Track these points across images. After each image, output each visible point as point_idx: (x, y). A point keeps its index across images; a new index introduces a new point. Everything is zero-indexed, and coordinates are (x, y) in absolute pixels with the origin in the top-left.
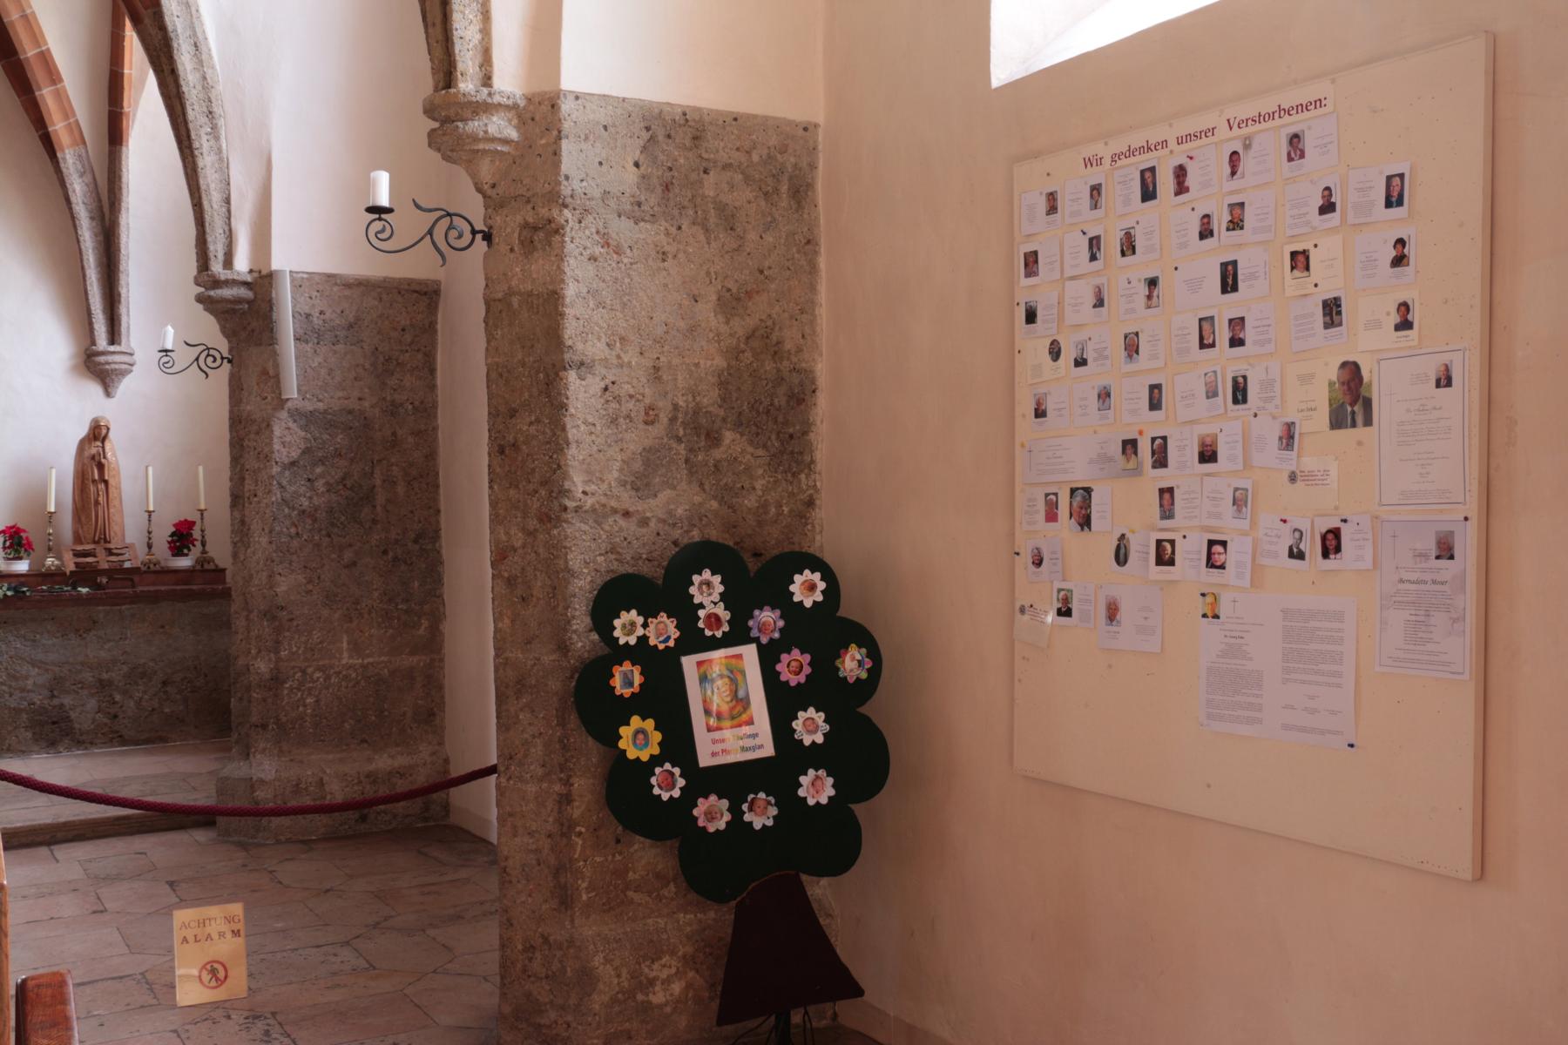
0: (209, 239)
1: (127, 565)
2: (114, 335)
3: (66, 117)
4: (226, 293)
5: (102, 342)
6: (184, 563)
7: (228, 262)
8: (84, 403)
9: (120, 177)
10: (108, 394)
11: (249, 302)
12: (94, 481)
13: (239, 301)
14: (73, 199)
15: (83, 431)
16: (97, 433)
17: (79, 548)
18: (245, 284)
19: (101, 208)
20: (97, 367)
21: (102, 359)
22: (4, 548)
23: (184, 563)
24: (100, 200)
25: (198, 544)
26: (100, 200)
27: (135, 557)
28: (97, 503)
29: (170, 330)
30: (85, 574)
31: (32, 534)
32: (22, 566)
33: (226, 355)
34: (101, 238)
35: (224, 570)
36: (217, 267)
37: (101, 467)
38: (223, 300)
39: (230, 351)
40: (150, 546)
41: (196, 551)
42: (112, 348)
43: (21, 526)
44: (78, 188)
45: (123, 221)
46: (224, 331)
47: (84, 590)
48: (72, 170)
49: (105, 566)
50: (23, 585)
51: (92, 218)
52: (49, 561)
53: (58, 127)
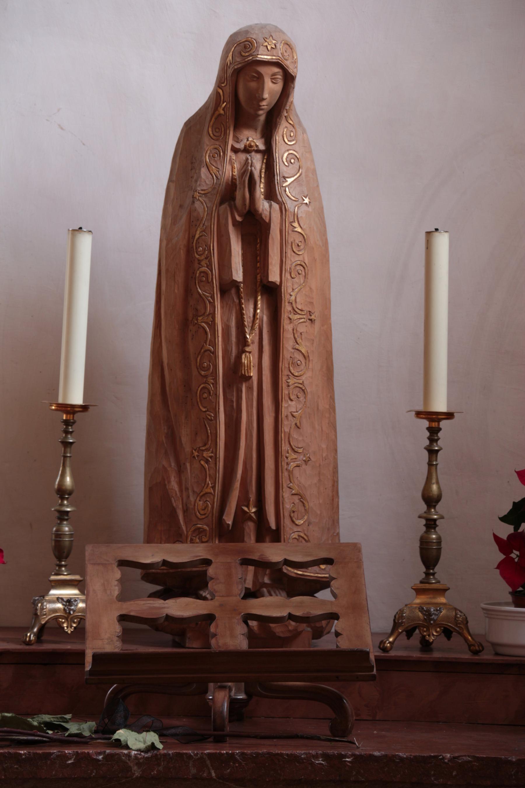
12: (228, 287)
15: (196, 88)
17: (152, 555)
28: (236, 375)
30: (157, 673)
37: (255, 231)
40: (430, 555)
47: (135, 741)
49: (232, 637)
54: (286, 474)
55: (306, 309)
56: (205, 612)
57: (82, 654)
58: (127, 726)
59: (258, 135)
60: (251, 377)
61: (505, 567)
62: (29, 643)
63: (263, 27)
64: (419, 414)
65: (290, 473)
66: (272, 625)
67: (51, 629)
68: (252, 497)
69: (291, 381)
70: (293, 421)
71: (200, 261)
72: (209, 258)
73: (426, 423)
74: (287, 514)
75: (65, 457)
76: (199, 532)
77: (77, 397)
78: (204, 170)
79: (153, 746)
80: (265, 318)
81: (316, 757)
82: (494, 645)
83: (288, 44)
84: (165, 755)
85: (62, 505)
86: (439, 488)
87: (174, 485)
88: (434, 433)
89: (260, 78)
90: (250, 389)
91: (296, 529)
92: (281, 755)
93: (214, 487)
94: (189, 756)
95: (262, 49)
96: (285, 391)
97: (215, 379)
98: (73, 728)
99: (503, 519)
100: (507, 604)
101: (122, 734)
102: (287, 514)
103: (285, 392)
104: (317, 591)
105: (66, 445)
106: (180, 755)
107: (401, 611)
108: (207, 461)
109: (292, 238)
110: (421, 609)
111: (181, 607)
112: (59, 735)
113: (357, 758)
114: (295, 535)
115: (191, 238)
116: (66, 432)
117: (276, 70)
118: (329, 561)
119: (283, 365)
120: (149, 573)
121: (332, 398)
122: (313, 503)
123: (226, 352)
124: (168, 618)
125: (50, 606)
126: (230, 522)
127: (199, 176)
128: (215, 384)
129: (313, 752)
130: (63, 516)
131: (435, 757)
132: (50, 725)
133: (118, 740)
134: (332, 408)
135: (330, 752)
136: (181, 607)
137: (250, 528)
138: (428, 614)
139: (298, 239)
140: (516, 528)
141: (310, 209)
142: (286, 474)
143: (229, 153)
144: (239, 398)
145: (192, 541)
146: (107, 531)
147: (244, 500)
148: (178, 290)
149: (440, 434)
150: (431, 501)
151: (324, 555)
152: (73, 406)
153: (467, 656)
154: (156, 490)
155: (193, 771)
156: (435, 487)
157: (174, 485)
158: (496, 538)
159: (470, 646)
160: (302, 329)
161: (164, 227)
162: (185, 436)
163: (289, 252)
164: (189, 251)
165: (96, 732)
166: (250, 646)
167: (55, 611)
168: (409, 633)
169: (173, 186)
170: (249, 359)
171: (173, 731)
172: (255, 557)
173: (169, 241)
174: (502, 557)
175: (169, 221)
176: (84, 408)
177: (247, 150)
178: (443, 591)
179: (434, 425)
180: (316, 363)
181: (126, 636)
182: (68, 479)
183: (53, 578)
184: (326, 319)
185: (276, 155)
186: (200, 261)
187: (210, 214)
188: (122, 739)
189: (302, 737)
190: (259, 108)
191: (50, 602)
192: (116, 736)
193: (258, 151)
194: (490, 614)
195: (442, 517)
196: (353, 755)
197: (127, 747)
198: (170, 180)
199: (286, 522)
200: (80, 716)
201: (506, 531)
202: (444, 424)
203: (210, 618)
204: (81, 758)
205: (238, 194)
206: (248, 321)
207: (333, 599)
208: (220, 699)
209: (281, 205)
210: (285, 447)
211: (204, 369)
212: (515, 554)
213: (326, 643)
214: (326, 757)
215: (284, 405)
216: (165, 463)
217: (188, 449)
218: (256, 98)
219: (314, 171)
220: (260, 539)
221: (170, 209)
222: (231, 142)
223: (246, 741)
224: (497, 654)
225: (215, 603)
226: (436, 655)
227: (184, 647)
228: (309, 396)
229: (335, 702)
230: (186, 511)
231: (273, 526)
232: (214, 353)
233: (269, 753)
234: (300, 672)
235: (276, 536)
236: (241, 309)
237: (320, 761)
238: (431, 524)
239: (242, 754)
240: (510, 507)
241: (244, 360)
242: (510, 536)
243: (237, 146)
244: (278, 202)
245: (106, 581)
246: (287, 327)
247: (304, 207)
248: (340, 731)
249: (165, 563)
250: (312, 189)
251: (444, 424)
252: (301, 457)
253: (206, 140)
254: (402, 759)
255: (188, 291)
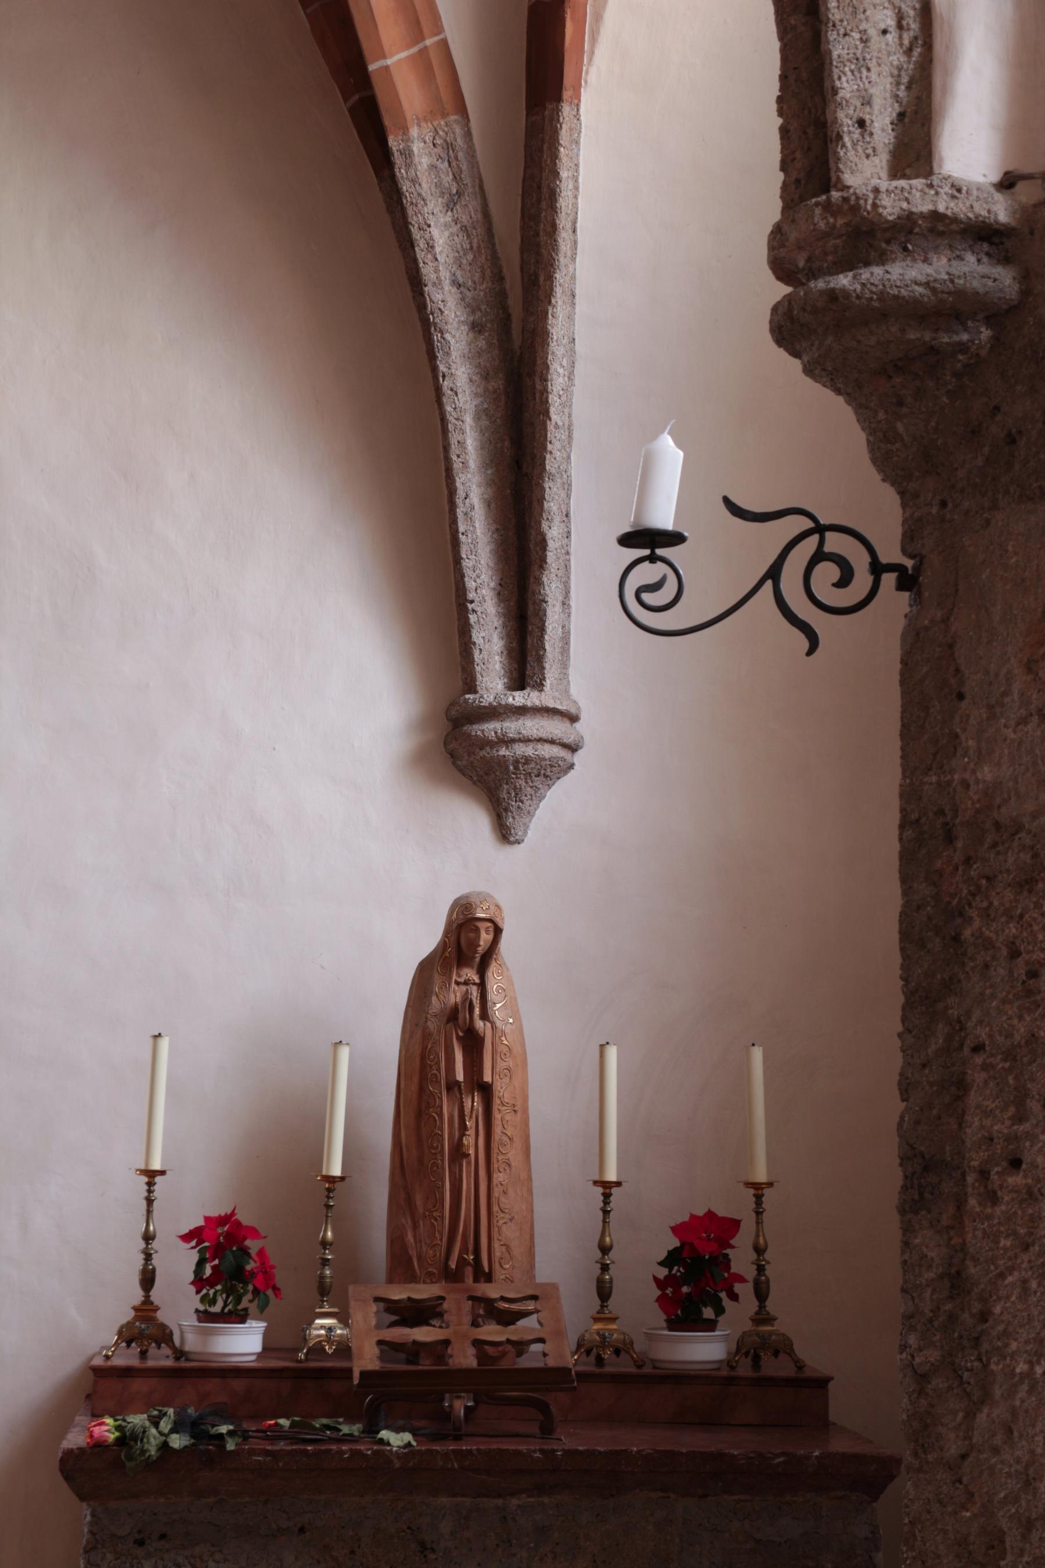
0: (839, 48)
1: (533, 1358)
2: (525, 664)
3: (416, 32)
4: (904, 274)
5: (492, 683)
6: (704, 1349)
7: (915, 147)
8: (437, 857)
9: (553, 196)
10: (505, 834)
11: (997, 314)
12: (452, 1086)
13: (951, 307)
14: (427, 272)
15: (428, 937)
16: (467, 941)
17: (398, 1293)
18: (983, 235)
19: (499, 298)
20: (476, 755)
21: (490, 728)
22: (199, 1282)
23: (704, 1349)
24: (499, 277)
25: (557, 520)
26: (499, 277)
27: (556, 1334)
28: (458, 1153)
29: (670, 456)
30: (408, 1385)
31: (273, 1245)
32: (244, 1342)
33: (891, 553)
34: (498, 383)
35: (821, 1383)
36: (865, 171)
37: (473, 1044)
38: (892, 308)
39: (910, 537)
40: (604, 1292)
41: (738, 1314)
42: (518, 698)
43: (245, 1218)
44: (441, 239)
45: (557, 326)
46: (889, 457)
47: (396, 1439)
48: (426, 185)
49: (465, 1358)
50: (222, 1414)
51: (476, 327)
52: (322, 1324)
53: (393, 60)
54: (496, 1229)
55: (511, 1102)
56: (442, 1338)
57: (350, 1371)
58: (387, 1428)
59: (475, 972)
60: (469, 1155)
61: (662, 1301)
62: (301, 1361)
63: (479, 893)
64: (596, 1183)
65: (499, 1228)
66: (486, 1347)
67: (317, 1350)
68: (471, 1247)
69: (500, 1157)
70: (501, 1188)
71: (431, 1066)
72: (438, 1063)
73: (600, 1190)
74: (497, 1260)
75: (327, 1216)
76: (430, 1274)
77: (336, 1171)
78: (434, 998)
79: (409, 1444)
80: (480, 1110)
81: (535, 1451)
82: (653, 1361)
83: (498, 906)
84: (419, 1451)
85: (324, 1253)
86: (611, 1240)
87: (410, 1238)
88: (607, 1196)
89: (477, 930)
90: (469, 1163)
91: (504, 1272)
92: (508, 1450)
93: (441, 1240)
94: (437, 1451)
95: (479, 909)
96: (495, 1165)
97: (443, 1155)
98: (345, 1429)
99: (661, 1264)
100: (662, 1329)
101: (384, 1434)
102: (497, 1260)
103: (496, 1166)
104: (518, 1320)
105: (328, 1207)
106: (430, 1451)
107: (583, 1335)
108: (436, 1220)
109: (501, 1048)
110: (598, 1334)
111: (422, 1334)
112: (334, 1435)
113: (567, 1453)
114: (503, 1277)
115: (424, 1048)
116: (328, 1197)
117: (489, 924)
118: (534, 1298)
119: (494, 1145)
120: (390, 1306)
121: (530, 1171)
122: (517, 1251)
123: (451, 1135)
124: (414, 1342)
125: (315, 1332)
126: (454, 1267)
127: (430, 1003)
128: (443, 1160)
129: (533, 1448)
130: (325, 1262)
131: (625, 1450)
132: (327, 1427)
133: (382, 1439)
134: (530, 1179)
135: (545, 1447)
136: (422, 1334)
137: (469, 1272)
138: (603, 1337)
139: (505, 1049)
140: (670, 1270)
141: (514, 1027)
142: (496, 1229)
143: (453, 985)
144: (461, 1170)
145: (424, 1282)
146: (353, 1271)
147: (464, 1249)
148: (414, 1088)
149: (612, 1198)
150: (605, 1250)
151: (530, 1292)
152: (334, 1177)
153: (633, 1370)
154: (396, 1241)
155: (441, 1463)
156: (608, 1239)
157: (410, 1238)
158: (655, 1279)
159: (635, 1362)
160: (508, 1117)
161: (403, 1040)
162: (419, 1200)
163: (499, 1059)
164: (423, 1058)
165: (363, 1432)
166: (479, 1365)
167: (319, 1336)
168: (588, 1352)
169: (410, 1009)
170: (469, 1141)
171: (422, 1432)
172: (479, 1294)
173: (407, 1051)
174: (659, 1293)
175: (407, 1036)
176: (342, 1179)
177: (466, 983)
178: (613, 1320)
179: (608, 1191)
180: (518, 1143)
181: (382, 1358)
182: (329, 1234)
183: (318, 1310)
184: (525, 1110)
185: (488, 987)
186: (431, 1066)
187: (439, 1031)
188: (385, 1438)
189: (521, 1436)
190: (476, 952)
191: (316, 1329)
192: (380, 1436)
193: (474, 984)
194: (649, 1336)
195: (613, 1262)
196: (563, 1450)
197: (389, 1444)
198: (408, 1005)
199: (496, 1266)
200: (350, 1420)
201: (663, 1273)
202: (614, 1190)
203: (446, 1343)
204: (355, 1453)
205: (460, 1016)
206: (467, 1111)
207: (538, 1326)
208: (459, 1406)
209: (493, 1024)
210: (495, 1208)
211: (433, 1148)
212: (669, 1291)
213: (525, 1362)
214: (542, 1451)
215: (495, 1176)
216: (403, 1221)
217: (421, 1210)
218: (474, 944)
219: (515, 999)
220: (476, 1280)
221: (408, 1026)
222: (454, 977)
223: (478, 1439)
224: (655, 1368)
225: (451, 1330)
226: (608, 1369)
227: (417, 1364)
228: (513, 1169)
229: (543, 1408)
230: (419, 1258)
231: (487, 1270)
232: (442, 1136)
233: (499, 1449)
234: (511, 1386)
235: (489, 1278)
236: (462, 1102)
237: (538, 1455)
238: (605, 1268)
239: (478, 1450)
240: (666, 1254)
241: (465, 1142)
242: (666, 1277)
243: (459, 980)
244: (490, 1021)
245: (366, 1316)
246: (497, 1116)
247: (509, 1026)
248: (547, 1430)
249: (409, 1298)
250: (516, 1014)
251: (614, 1190)
252: (508, 1216)
253: (436, 976)
254: (600, 1452)
255: (422, 1089)
